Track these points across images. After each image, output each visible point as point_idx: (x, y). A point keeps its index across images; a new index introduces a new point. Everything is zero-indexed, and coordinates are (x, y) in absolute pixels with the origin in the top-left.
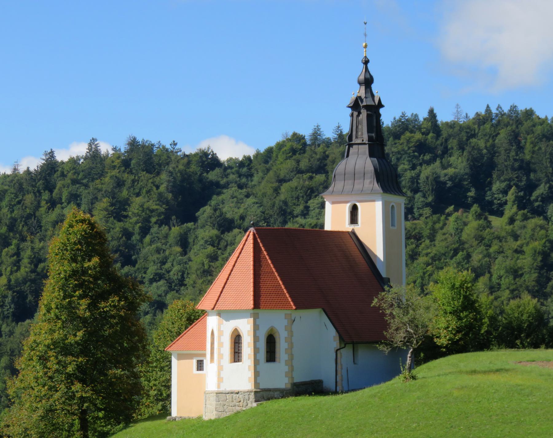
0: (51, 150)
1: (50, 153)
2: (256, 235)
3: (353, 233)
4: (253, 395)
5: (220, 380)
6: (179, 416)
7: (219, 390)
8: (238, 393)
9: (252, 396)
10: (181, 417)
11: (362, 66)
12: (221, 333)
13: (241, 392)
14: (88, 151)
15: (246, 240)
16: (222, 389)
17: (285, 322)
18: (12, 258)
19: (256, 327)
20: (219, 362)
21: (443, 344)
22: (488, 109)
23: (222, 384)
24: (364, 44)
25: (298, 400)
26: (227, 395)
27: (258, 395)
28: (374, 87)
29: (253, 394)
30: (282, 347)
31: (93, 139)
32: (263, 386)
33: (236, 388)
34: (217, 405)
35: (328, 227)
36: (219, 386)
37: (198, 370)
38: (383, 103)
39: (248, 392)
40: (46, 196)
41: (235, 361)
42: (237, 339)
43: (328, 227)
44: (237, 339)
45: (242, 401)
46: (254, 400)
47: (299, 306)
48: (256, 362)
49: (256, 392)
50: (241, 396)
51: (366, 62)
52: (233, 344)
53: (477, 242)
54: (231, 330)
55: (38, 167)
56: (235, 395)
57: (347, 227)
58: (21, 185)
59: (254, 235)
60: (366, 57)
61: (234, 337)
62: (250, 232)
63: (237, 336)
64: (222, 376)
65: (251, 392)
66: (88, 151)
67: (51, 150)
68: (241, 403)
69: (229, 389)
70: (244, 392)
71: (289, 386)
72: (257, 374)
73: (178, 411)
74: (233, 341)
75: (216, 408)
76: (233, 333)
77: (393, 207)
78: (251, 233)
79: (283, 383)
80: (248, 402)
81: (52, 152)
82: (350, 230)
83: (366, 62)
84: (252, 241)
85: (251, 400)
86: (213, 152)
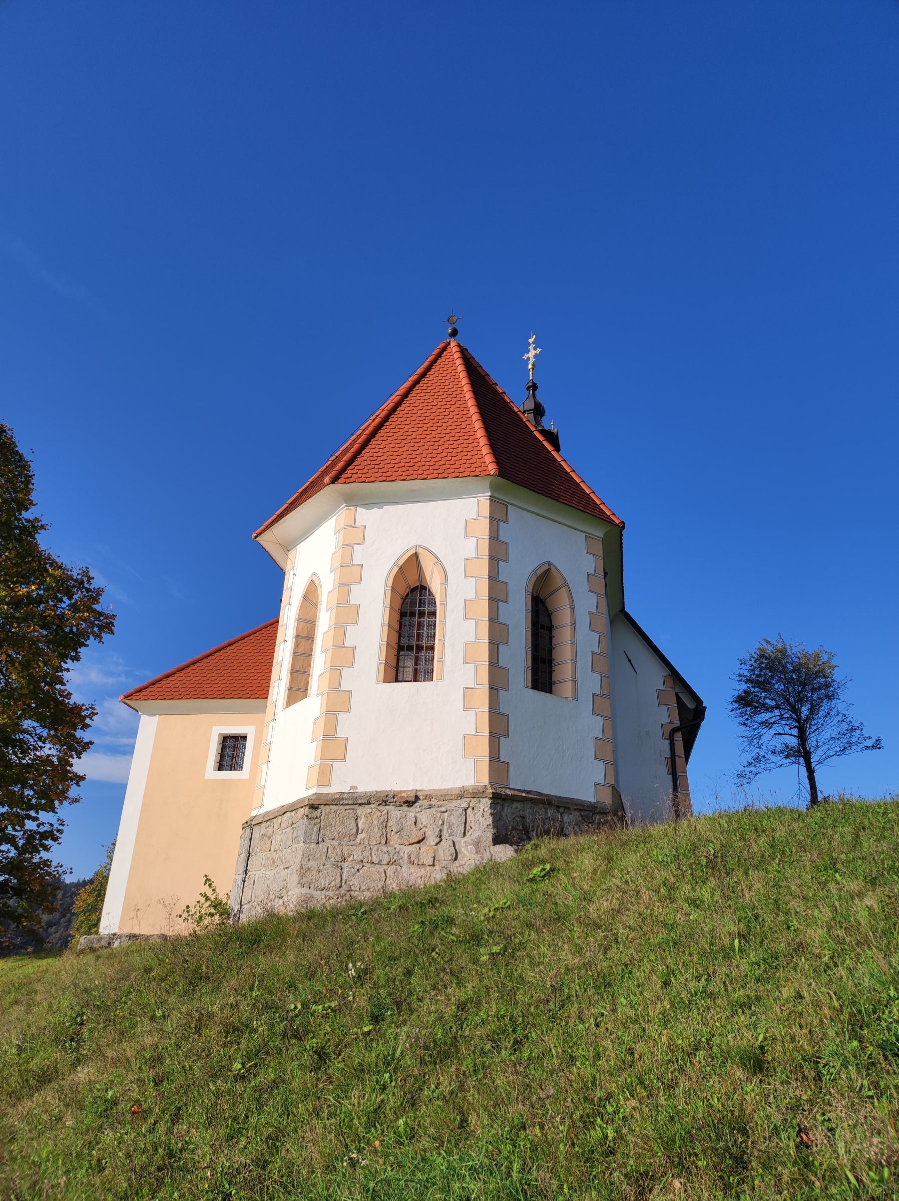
4: (488, 811)
6: (127, 930)
7: (325, 790)
8: (410, 803)
10: (133, 937)
13: (428, 797)
16: (338, 786)
26: (362, 811)
27: (508, 811)
28: (537, 392)
29: (485, 803)
34: (308, 856)
39: (461, 796)
45: (432, 840)
46: (489, 835)
50: (425, 817)
52: (397, 617)
53: (747, 673)
54: (399, 553)
56: (395, 813)
61: (403, 590)
63: (413, 590)
65: (477, 794)
68: (424, 847)
69: (366, 787)
70: (445, 796)
73: (132, 909)
74: (397, 606)
75: (303, 871)
76: (402, 572)
80: (461, 843)
85: (473, 834)
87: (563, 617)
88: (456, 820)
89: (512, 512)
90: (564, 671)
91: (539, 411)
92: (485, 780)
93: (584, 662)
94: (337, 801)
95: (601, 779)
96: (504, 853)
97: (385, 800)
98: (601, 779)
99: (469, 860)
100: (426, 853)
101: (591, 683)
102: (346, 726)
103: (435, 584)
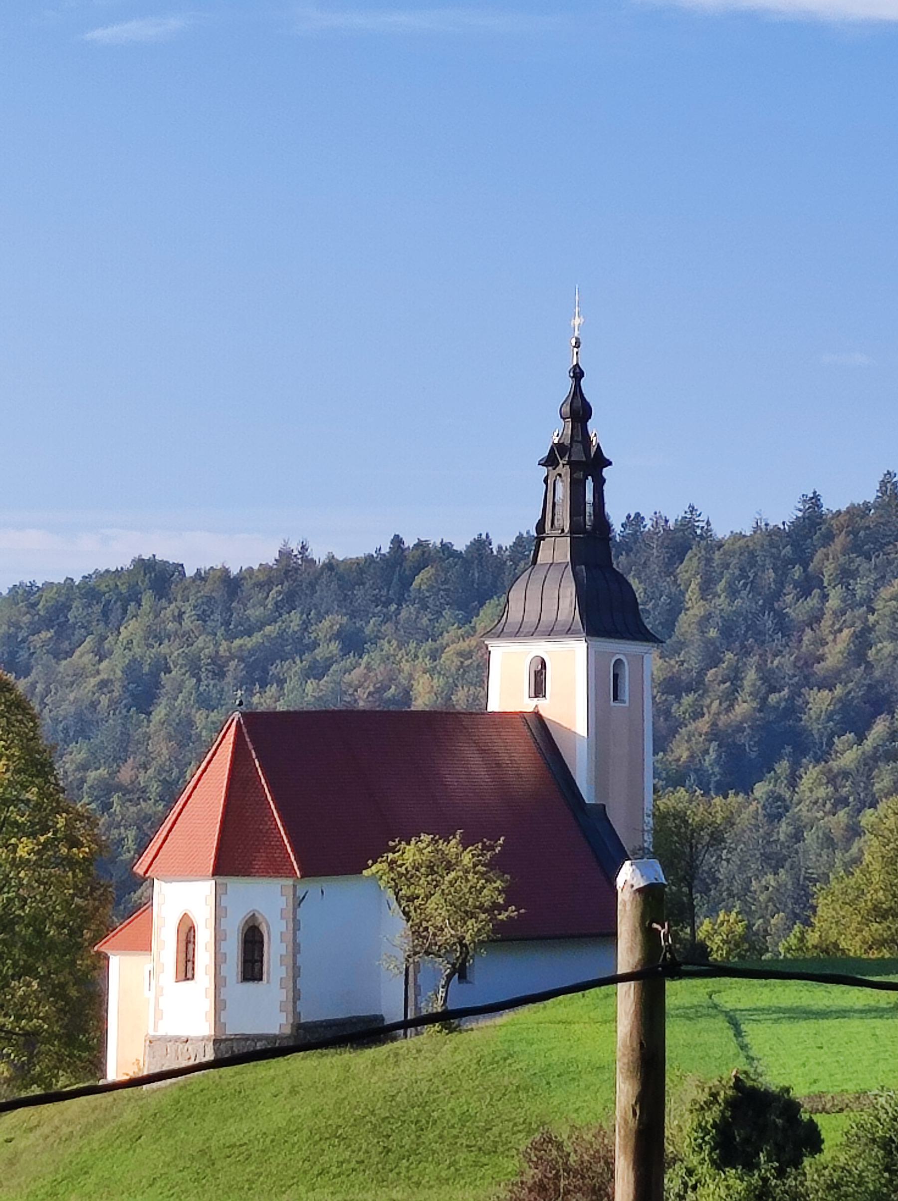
0: (815, 493)
1: (812, 498)
2: (243, 727)
3: (537, 715)
11: (570, 383)
14: (880, 494)
16: (161, 1032)
18: (723, 686)
23: (161, 1023)
24: (573, 341)
25: (326, 1055)
31: (889, 473)
32: (232, 1030)
33: (184, 1033)
35: (494, 705)
37: (261, 979)
38: (606, 455)
40: (797, 572)
41: (187, 979)
43: (494, 705)
47: (311, 870)
48: (219, 982)
49: (216, 1041)
51: (578, 374)
55: (784, 523)
57: (528, 705)
58: (752, 555)
59: (239, 725)
60: (577, 364)
62: (233, 720)
65: (208, 1039)
66: (880, 494)
67: (815, 493)
71: (287, 1031)
72: (219, 1005)
77: (618, 663)
78: (234, 723)
81: (816, 497)
83: (578, 374)
86: (708, 523)
92: (213, 1033)
94: (160, 1039)
97: (176, 1039)
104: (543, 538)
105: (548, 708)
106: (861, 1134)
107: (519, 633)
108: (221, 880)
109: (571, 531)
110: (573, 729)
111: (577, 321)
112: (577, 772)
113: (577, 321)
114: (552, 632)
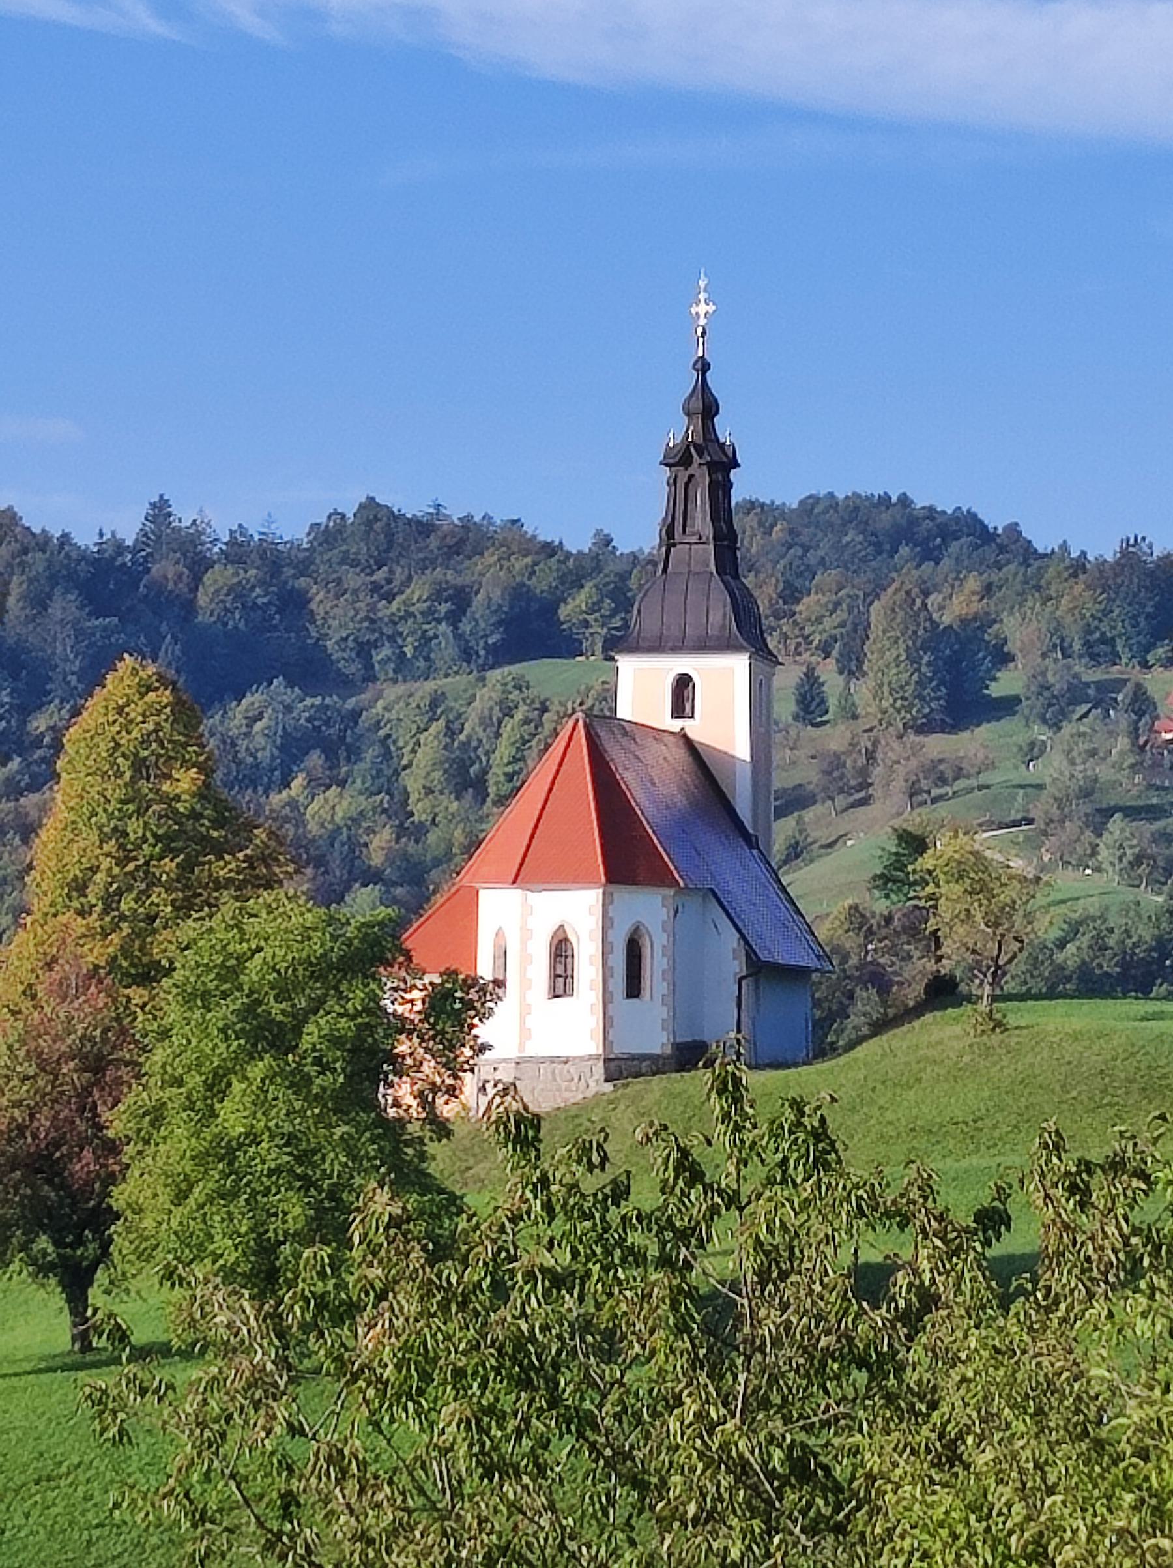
5: (525, 1034)
9: (599, 1070)
11: (691, 378)
12: (526, 934)
15: (574, 729)
16: (532, 1050)
17: (664, 914)
19: (607, 923)
20: (523, 997)
21: (929, 531)
22: (1064, 546)
27: (612, 1065)
29: (601, 1063)
30: (654, 966)
32: (617, 1050)
36: (521, 1047)
42: (561, 950)
44: (561, 950)
48: (607, 999)
51: (703, 366)
61: (555, 941)
64: (528, 1025)
65: (598, 1057)
70: (582, 1059)
78: (581, 723)
79: (658, 1043)
82: (677, 730)
83: (703, 366)
84: (582, 733)
85: (596, 1077)
87: (646, 952)
88: (588, 1070)
89: (616, 896)
90: (646, 983)
91: (526, 1108)
92: (601, 1051)
93: (658, 975)
94: (530, 1060)
95: (665, 1016)
96: (609, 1087)
97: (553, 1060)
98: (665, 1016)
99: (594, 1088)
100: (573, 1086)
101: (662, 988)
102: (530, 1022)
103: (572, 938)
104: (674, 545)
105: (695, 729)
106: (307, 1363)
107: (657, 646)
108: (612, 888)
109: (714, 538)
110: (731, 752)
111: (702, 309)
112: (738, 800)
113: (702, 309)
114: (705, 645)
